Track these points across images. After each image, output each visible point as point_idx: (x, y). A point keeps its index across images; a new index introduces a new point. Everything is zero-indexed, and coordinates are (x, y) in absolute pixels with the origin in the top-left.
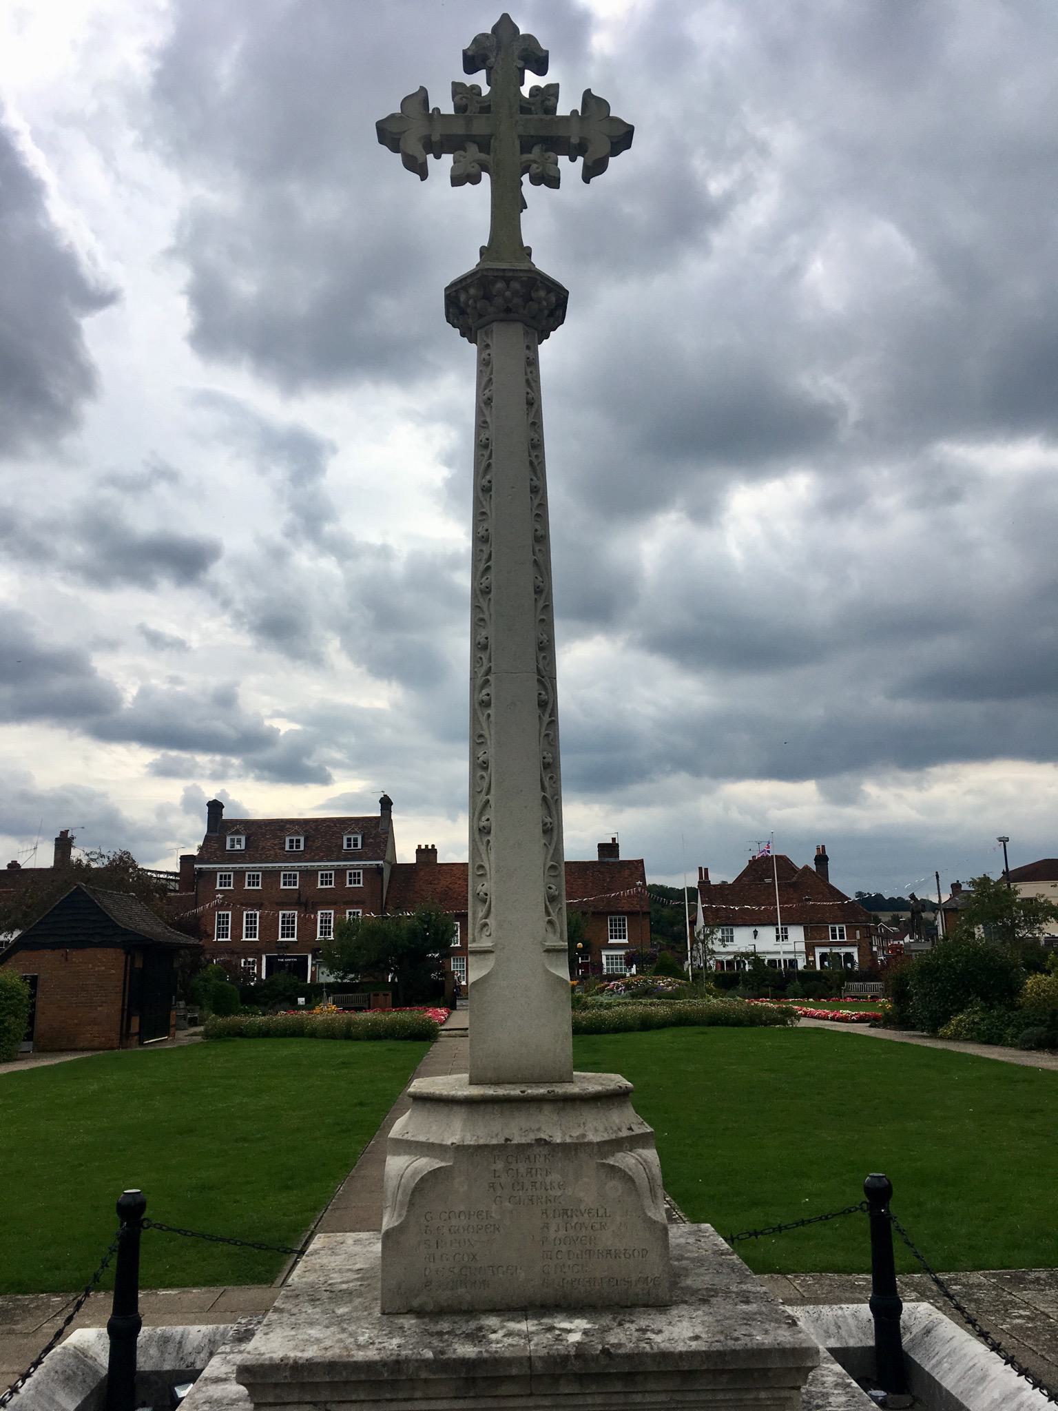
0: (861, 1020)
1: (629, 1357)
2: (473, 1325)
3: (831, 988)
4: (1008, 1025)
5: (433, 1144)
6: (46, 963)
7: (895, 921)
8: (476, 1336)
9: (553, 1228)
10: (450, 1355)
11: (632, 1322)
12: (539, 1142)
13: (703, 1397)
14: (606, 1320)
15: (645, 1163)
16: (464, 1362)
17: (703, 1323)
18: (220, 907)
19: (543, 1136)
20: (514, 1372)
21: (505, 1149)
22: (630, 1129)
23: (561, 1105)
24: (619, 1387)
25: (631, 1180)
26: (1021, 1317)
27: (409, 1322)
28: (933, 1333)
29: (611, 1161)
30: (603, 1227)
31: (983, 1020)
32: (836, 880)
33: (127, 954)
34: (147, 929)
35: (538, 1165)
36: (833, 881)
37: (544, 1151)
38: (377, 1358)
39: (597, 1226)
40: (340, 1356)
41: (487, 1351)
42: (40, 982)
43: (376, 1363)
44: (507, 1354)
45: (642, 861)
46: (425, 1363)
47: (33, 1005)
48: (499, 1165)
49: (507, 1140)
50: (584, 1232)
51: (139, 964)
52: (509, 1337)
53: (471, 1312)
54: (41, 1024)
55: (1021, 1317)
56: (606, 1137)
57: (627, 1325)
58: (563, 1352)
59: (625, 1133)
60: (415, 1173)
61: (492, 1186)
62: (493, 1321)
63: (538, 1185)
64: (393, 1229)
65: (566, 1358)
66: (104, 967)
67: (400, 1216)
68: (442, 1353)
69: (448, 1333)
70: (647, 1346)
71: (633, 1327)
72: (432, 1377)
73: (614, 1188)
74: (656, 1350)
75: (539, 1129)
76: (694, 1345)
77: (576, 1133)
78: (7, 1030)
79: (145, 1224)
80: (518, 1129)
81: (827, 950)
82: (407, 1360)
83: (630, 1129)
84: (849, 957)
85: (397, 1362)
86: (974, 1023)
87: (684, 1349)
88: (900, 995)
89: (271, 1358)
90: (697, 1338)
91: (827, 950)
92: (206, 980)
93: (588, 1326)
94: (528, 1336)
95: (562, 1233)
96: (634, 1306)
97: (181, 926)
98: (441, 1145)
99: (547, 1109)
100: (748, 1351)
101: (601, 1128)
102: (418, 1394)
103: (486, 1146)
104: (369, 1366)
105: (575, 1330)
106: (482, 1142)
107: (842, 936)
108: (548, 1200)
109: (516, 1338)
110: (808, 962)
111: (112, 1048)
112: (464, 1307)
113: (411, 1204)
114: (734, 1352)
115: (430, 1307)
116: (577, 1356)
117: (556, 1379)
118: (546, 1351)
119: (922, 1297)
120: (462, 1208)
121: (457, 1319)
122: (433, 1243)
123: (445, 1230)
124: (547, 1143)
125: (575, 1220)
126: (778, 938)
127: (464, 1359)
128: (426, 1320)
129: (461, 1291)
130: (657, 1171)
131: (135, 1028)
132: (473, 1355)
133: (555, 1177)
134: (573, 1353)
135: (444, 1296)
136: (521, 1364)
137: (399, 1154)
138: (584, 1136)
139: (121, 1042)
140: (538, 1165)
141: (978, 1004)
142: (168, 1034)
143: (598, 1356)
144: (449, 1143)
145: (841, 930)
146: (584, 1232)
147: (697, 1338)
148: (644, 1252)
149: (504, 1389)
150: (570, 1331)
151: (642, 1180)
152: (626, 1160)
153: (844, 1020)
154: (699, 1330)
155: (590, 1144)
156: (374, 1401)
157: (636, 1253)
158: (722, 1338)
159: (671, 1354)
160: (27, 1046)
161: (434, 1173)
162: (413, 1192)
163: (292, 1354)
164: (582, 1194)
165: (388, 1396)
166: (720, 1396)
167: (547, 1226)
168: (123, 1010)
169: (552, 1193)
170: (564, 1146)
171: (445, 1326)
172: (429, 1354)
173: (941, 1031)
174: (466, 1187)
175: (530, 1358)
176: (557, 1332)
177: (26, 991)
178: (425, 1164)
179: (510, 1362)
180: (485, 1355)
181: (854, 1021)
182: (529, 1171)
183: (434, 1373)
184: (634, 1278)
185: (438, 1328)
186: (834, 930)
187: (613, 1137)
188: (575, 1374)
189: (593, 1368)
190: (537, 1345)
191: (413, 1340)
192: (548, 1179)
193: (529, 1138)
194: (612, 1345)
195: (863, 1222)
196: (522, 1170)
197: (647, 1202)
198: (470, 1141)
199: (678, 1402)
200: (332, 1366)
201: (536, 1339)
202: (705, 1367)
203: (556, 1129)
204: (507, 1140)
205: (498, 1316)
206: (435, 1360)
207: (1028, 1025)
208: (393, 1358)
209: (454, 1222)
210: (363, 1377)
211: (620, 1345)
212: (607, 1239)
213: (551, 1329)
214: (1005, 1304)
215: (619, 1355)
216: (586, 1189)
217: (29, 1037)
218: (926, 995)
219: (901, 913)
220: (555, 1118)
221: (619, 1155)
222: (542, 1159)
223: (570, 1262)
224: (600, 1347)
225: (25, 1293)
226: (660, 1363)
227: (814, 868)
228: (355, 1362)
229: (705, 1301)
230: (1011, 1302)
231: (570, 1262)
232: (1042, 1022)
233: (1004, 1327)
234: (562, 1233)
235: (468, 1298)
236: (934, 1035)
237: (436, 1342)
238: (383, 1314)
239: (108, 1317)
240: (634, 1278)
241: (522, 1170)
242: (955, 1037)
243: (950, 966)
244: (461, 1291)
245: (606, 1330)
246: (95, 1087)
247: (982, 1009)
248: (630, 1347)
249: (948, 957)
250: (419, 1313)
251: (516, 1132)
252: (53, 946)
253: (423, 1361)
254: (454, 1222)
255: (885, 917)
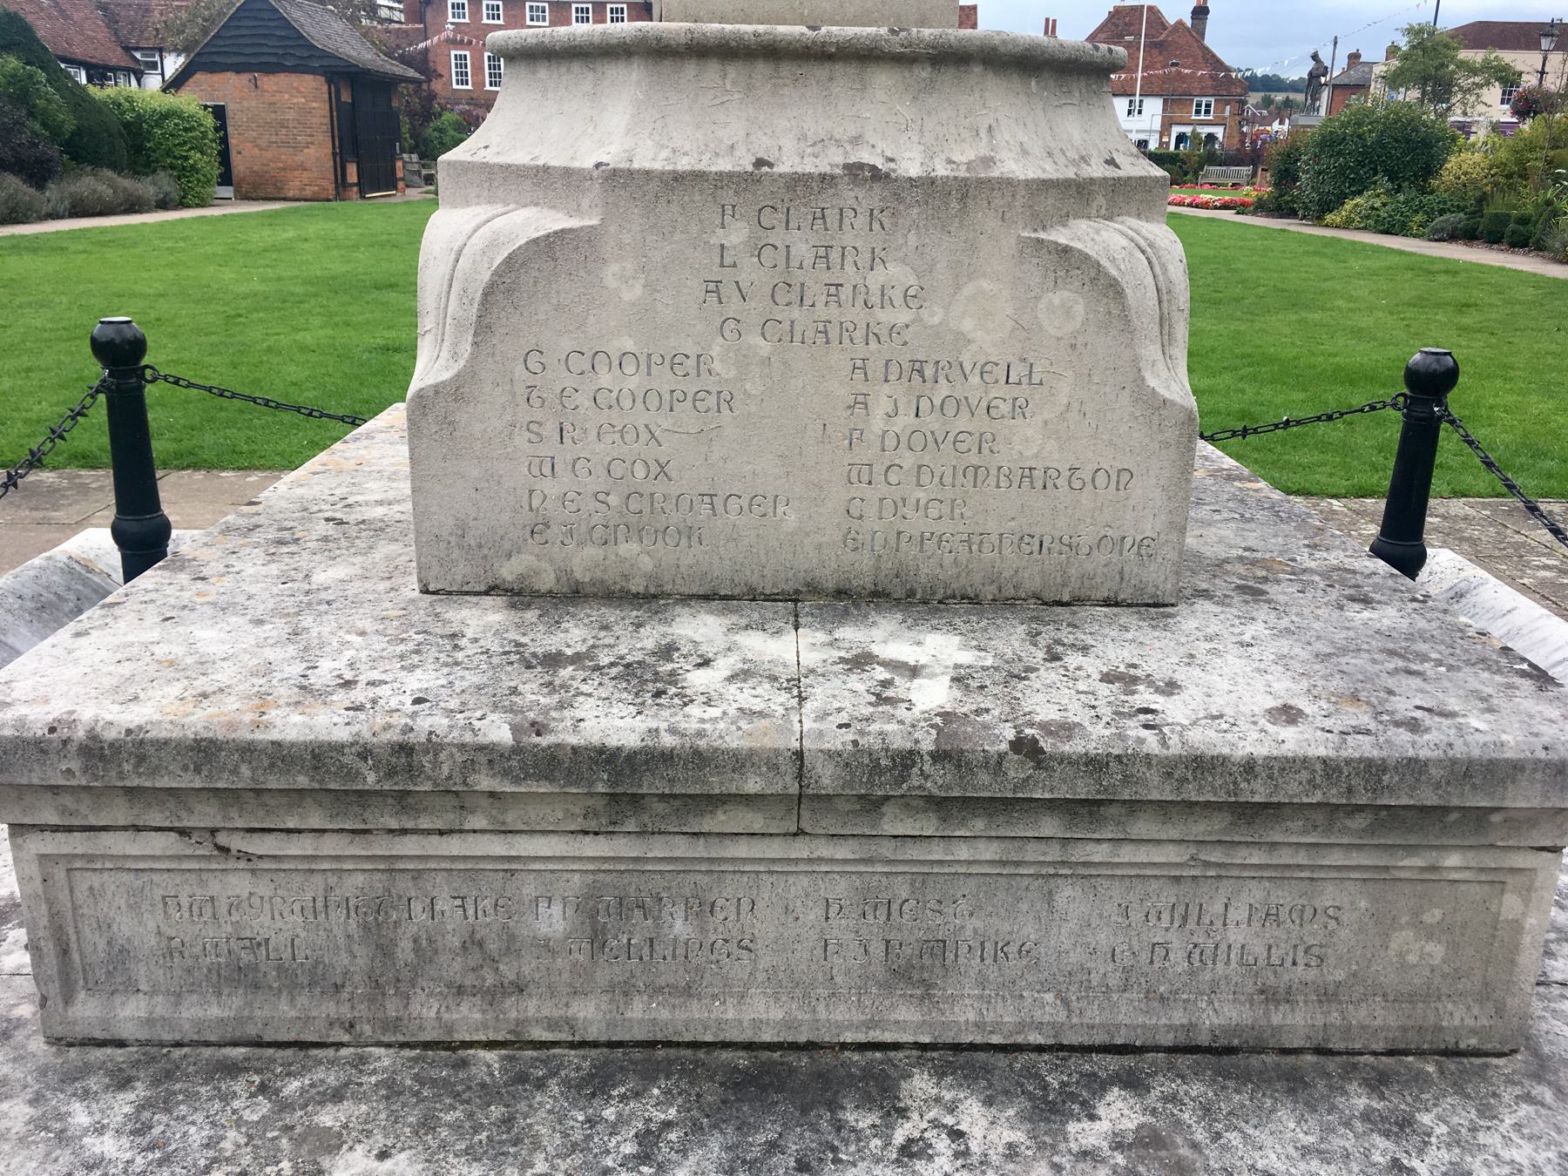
0: (1225, 206)
1: (1095, 764)
2: (650, 637)
3: (1186, 174)
4: (1416, 212)
5: (546, 169)
6: (229, 88)
7: (1267, 102)
8: (649, 679)
9: (881, 407)
10: (564, 735)
11: (1085, 650)
12: (855, 171)
13: (1285, 857)
14: (1011, 639)
15: (1150, 253)
16: (605, 758)
17: (1281, 658)
18: (454, 43)
19: (867, 157)
20: (753, 785)
21: (755, 188)
22: (1111, 162)
23: (924, 72)
24: (1050, 826)
25: (1114, 290)
26: (1546, 567)
27: (483, 621)
28: (1470, 599)
29: (1061, 236)
30: (1019, 409)
31: (1384, 205)
32: (1216, 39)
33: (329, 82)
34: (354, 54)
35: (848, 238)
36: (1210, 41)
37: (870, 198)
38: (342, 735)
39: (1005, 408)
40: (231, 726)
41: (673, 731)
42: (229, 113)
43: (339, 748)
44: (734, 742)
45: (974, 8)
46: (490, 755)
47: (224, 141)
48: (737, 235)
49: (760, 163)
50: (963, 422)
51: (346, 97)
52: (747, 686)
53: (651, 599)
54: (239, 164)
55: (1546, 567)
56: (1051, 171)
57: (1073, 660)
58: (899, 743)
59: (1097, 170)
60: (493, 244)
61: (714, 288)
62: (699, 628)
63: (846, 292)
64: (437, 389)
65: (906, 760)
66: (301, 100)
67: (455, 356)
68: (539, 729)
69: (577, 659)
70: (1151, 737)
71: (1093, 666)
72: (509, 788)
73: (1063, 310)
74: (1175, 748)
75: (856, 140)
76: (1291, 740)
77: (965, 154)
78: (193, 168)
79: (148, 373)
80: (795, 131)
81: (1188, 130)
82: (433, 746)
83: (1111, 162)
84: (1211, 138)
85: (404, 749)
86: (1373, 208)
87: (1261, 751)
88: (1286, 176)
89: (21, 723)
90: (1288, 714)
91: (1188, 130)
92: (441, 131)
93: (967, 657)
94: (796, 687)
95: (905, 421)
96: (1077, 601)
97: (405, 60)
98: (567, 172)
99: (882, 79)
100: (1454, 762)
101: (1036, 148)
102: (478, 822)
103: (698, 176)
104: (319, 756)
105: (931, 673)
106: (684, 164)
107: (1208, 112)
108: (871, 334)
109: (765, 688)
110: (1161, 143)
111: (328, 200)
112: (637, 585)
113: (483, 328)
114: (1414, 767)
115: (547, 582)
116: (938, 756)
117: (872, 805)
118: (849, 736)
119: (1445, 544)
120: (629, 345)
121: (611, 615)
122: (550, 430)
123: (583, 400)
124: (876, 175)
125: (943, 389)
126: (1129, 112)
127: (602, 750)
128: (531, 615)
129: (629, 549)
130: (1178, 272)
131: (352, 177)
132: (631, 741)
133: (896, 274)
134: (927, 745)
135: (584, 561)
136: (776, 767)
137: (468, 204)
138: (988, 161)
139: (338, 194)
140: (848, 238)
141: (1384, 182)
142: (396, 188)
143: (1001, 756)
144: (588, 163)
145: (1208, 105)
146: (963, 422)
147: (1288, 714)
148: (1124, 476)
149: (720, 821)
150: (914, 671)
151: (1141, 297)
152: (1103, 238)
153: (1205, 206)
154: (1286, 688)
155: (1007, 183)
156: (353, 831)
157: (1101, 479)
158: (1365, 720)
159: (1223, 760)
160: (227, 191)
161: (548, 246)
162: (486, 295)
163: (87, 714)
164: (967, 325)
165: (394, 825)
166: (1336, 858)
167: (862, 402)
168: (334, 154)
169: (885, 316)
170: (928, 185)
171: (573, 635)
172: (498, 731)
173: (1329, 218)
174: (638, 291)
175: (799, 755)
176: (881, 674)
177: (209, 121)
178: (528, 222)
179: (740, 761)
180: (668, 741)
181: (1216, 208)
182: (823, 255)
183: (517, 780)
184: (1086, 538)
185: (552, 642)
186: (1199, 105)
187: (1070, 173)
188: (930, 799)
189: (984, 785)
190: (823, 716)
191: (473, 678)
192: (876, 279)
193: (830, 161)
194: (1045, 727)
195: (1392, 426)
196: (802, 249)
197: (1150, 351)
198: (650, 157)
199: (1207, 864)
200: (204, 751)
201: (819, 696)
202: (1317, 797)
203: (905, 134)
204: (760, 163)
205: (723, 612)
206: (517, 750)
207: (1442, 212)
208: (394, 736)
209: (605, 379)
210: (303, 781)
211: (1067, 730)
212: (1027, 441)
213: (860, 661)
214: (1518, 546)
215: (1063, 759)
216: (982, 306)
217: (226, 179)
218: (1320, 173)
219: (1273, 95)
220: (906, 110)
221: (1082, 226)
222: (862, 220)
223: (922, 495)
224: (1010, 734)
225: (93, 468)
226: (1183, 781)
227: (1189, 23)
228: (277, 744)
229: (1253, 593)
230: (1524, 544)
231: (922, 495)
232: (1460, 209)
233: (1525, 581)
234: (905, 421)
235: (647, 564)
236: (1318, 219)
237: (532, 692)
238: (425, 591)
239: (111, 514)
240: (1086, 538)
241: (802, 249)
242: (1346, 225)
243: (1360, 136)
244: (629, 549)
245: (1017, 674)
246: (291, 234)
247: (1387, 192)
248: (1096, 737)
249: (1359, 124)
250: (518, 595)
251: (789, 144)
252: (239, 69)
253: (481, 748)
254: (605, 379)
255: (1254, 98)
